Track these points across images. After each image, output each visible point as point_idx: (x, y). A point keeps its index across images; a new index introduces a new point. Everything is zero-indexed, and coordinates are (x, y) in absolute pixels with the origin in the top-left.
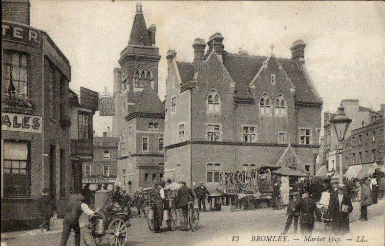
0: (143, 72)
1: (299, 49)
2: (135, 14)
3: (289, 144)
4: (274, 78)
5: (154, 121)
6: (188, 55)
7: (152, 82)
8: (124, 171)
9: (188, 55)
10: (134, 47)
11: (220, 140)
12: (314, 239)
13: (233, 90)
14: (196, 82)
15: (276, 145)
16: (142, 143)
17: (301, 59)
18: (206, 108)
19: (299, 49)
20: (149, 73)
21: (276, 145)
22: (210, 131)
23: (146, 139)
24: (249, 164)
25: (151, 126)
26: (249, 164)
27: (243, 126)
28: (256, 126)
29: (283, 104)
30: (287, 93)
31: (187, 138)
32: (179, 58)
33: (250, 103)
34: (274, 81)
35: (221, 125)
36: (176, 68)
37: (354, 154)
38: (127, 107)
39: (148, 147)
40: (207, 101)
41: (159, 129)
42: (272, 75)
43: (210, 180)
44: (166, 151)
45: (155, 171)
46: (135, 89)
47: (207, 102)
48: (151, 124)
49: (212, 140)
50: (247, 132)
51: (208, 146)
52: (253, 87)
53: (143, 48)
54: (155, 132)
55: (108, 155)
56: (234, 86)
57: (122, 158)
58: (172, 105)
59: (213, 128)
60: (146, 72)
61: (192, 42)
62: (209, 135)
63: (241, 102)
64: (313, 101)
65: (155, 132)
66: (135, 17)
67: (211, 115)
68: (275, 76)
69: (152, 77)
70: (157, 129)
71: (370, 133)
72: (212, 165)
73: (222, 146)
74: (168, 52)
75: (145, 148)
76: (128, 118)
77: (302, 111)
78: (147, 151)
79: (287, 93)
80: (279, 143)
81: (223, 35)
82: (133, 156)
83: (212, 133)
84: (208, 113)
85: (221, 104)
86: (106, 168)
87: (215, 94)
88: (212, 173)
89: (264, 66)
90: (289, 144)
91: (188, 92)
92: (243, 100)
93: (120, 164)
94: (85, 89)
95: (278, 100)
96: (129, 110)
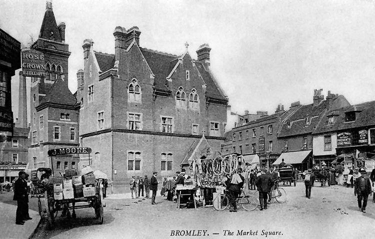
0: (54, 66)
1: (204, 53)
2: (46, 11)
3: (203, 135)
4: (188, 75)
5: (65, 112)
6: (108, 46)
7: (63, 77)
8: (35, 158)
9: (108, 46)
11: (140, 129)
12: (276, 233)
13: (152, 82)
14: (118, 70)
15: (191, 136)
16: (54, 132)
17: (207, 61)
18: (126, 97)
19: (204, 53)
20: (59, 67)
21: (191, 136)
22: (131, 120)
23: (58, 128)
24: (167, 153)
25: (63, 117)
26: (167, 153)
27: (161, 116)
28: (173, 118)
29: (196, 98)
30: (199, 89)
31: (108, 125)
32: (96, 48)
33: (167, 95)
35: (141, 114)
36: (94, 56)
37: (234, 147)
38: (37, 99)
39: (60, 136)
40: (128, 89)
41: (70, 120)
43: (130, 168)
44: (82, 139)
45: (66, 159)
47: (128, 91)
48: (62, 114)
49: (132, 128)
50: (164, 122)
51: (129, 134)
52: (170, 80)
54: (67, 123)
55: (17, 144)
57: (33, 146)
58: (90, 94)
59: (134, 118)
60: (56, 66)
61: (113, 30)
62: (130, 123)
63: (160, 94)
64: (221, 98)
65: (67, 123)
66: (45, 15)
67: (132, 103)
69: (62, 71)
70: (68, 120)
71: (250, 130)
72: (132, 153)
73: (142, 135)
74: (84, 41)
75: (57, 137)
76: (39, 109)
77: (159, 99)
78: (59, 140)
79: (199, 89)
80: (193, 134)
81: (140, 30)
82: (45, 144)
83: (133, 122)
84: (129, 101)
85: (141, 93)
86: (14, 156)
87: (136, 83)
88: (165, 162)
89: (180, 61)
90: (203, 135)
91: (109, 80)
92: (162, 92)
93: (32, 152)
94: (5, 33)
95: (191, 94)
96: (40, 100)
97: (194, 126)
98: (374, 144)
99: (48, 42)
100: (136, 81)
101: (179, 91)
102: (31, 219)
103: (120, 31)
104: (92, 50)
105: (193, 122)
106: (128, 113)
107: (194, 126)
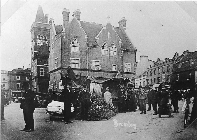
4: (110, 35)
7: (47, 41)
8: (137, 83)
10: (37, 23)
14: (64, 33)
34: (110, 36)
40: (71, 45)
42: (109, 33)
46: (38, 45)
47: (71, 46)
52: (98, 39)
53: (42, 24)
56: (87, 37)
68: (110, 34)
77: (126, 54)
84: (71, 52)
97: (113, 66)
98: (24, 98)
99: (39, 23)
100: (76, 40)
101: (74, 41)
102: (5, 119)
103: (65, 11)
104: (53, 24)
105: (113, 64)
106: (92, 60)
107: (113, 66)
